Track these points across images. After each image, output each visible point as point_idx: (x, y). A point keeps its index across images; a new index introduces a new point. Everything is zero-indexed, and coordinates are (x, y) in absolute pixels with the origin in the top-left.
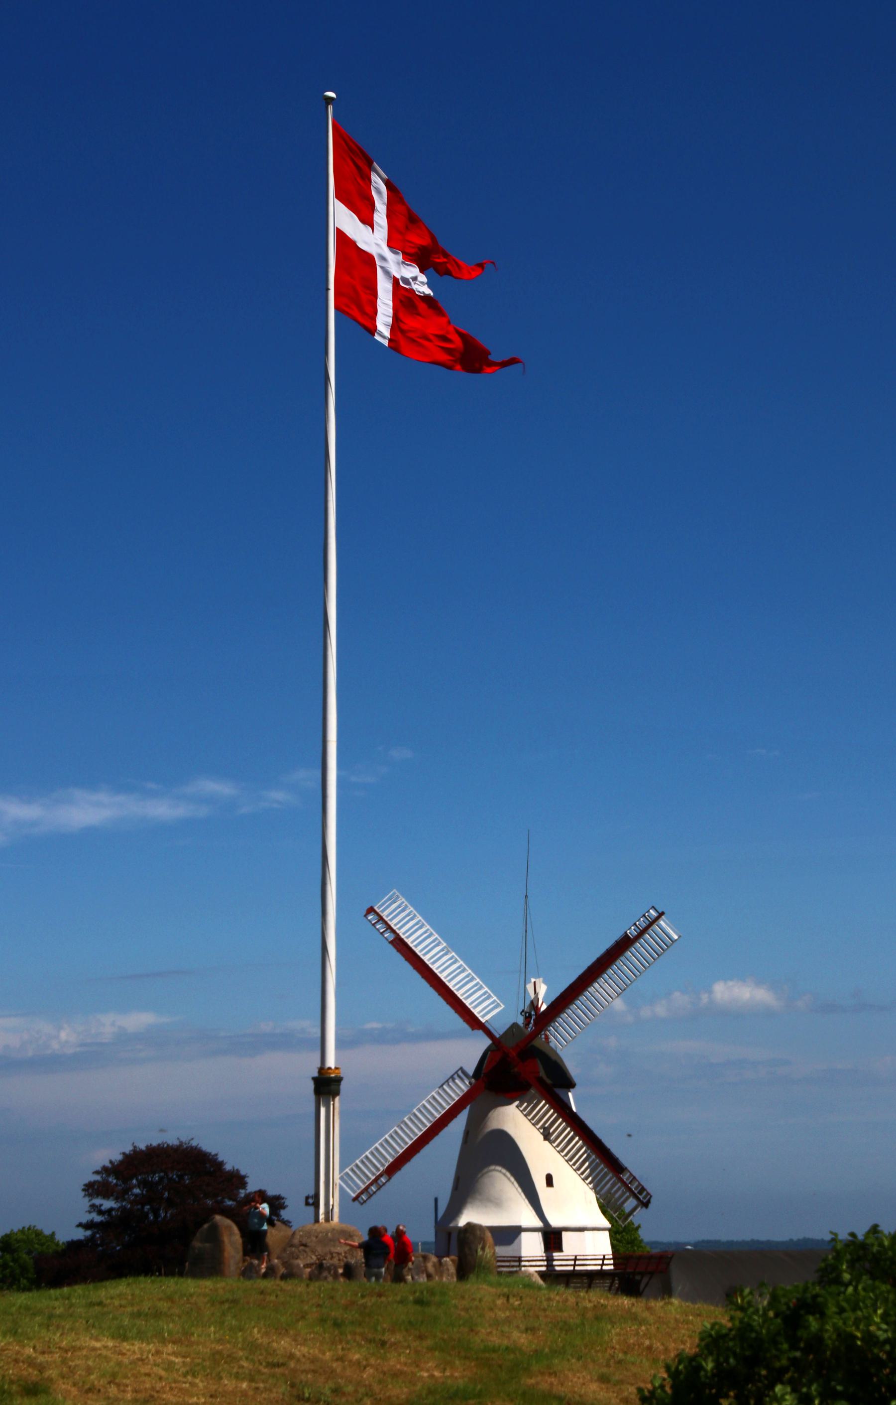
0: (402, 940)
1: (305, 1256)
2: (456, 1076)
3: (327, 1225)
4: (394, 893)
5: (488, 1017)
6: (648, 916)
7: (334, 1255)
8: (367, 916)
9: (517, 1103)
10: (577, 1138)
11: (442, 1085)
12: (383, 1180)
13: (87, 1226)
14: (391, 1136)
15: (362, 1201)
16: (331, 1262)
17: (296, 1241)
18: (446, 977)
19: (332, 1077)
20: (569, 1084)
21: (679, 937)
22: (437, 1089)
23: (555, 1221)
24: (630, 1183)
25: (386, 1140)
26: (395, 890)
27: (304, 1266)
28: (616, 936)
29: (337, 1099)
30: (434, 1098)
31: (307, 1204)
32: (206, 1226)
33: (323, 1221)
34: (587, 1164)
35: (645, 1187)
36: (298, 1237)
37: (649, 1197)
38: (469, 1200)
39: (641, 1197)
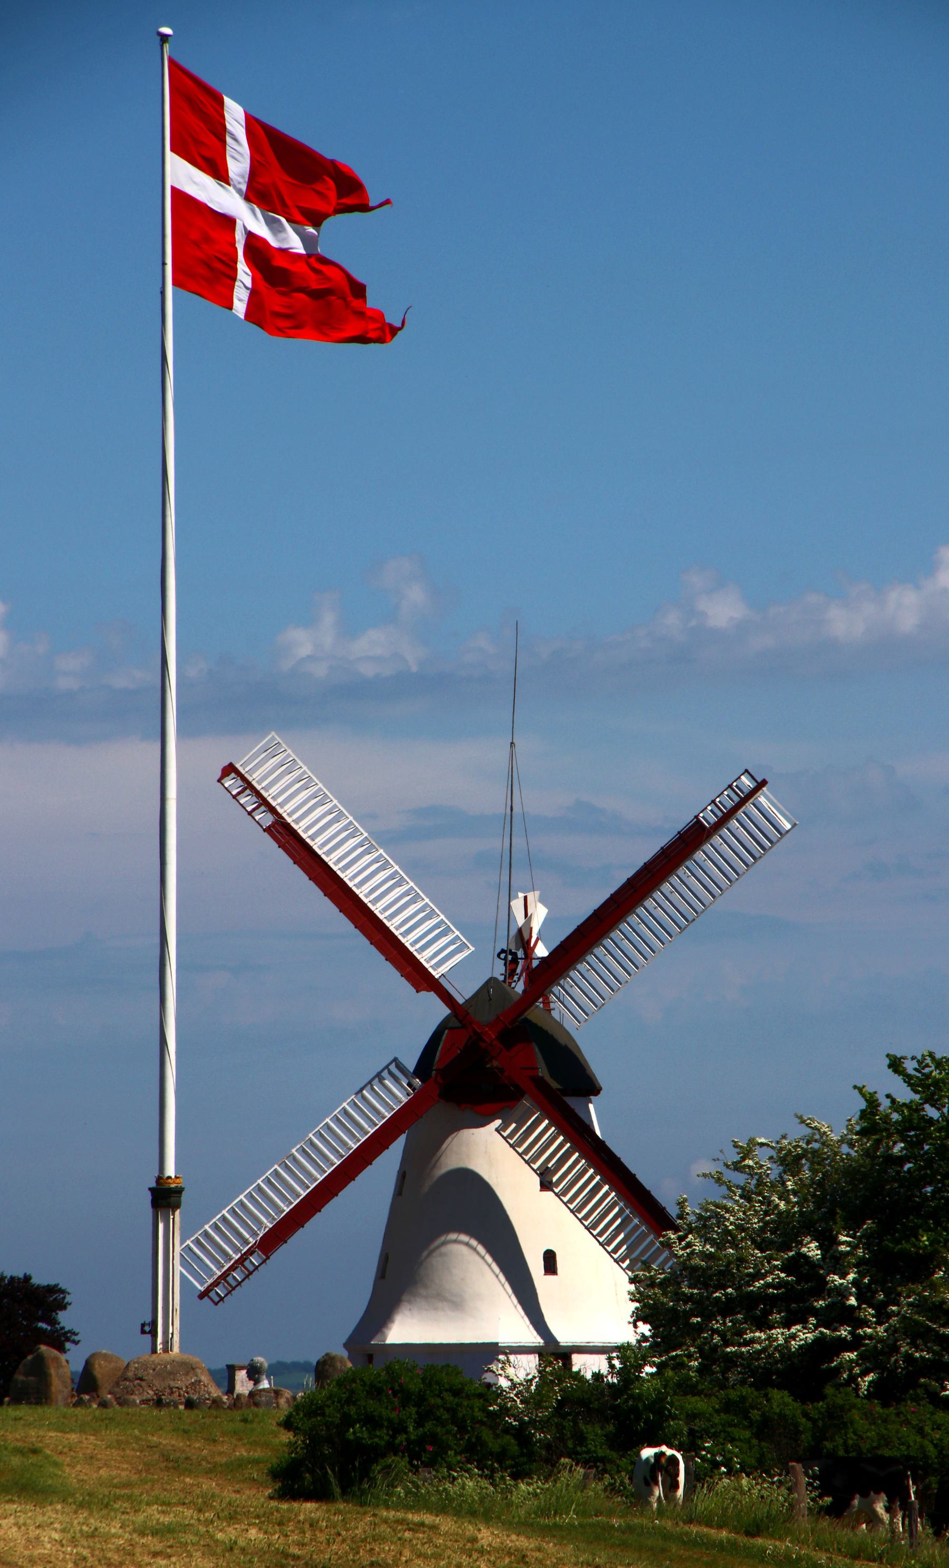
1: (141, 1391)
2: (385, 1074)
3: (165, 1356)
5: (444, 969)
6: (720, 802)
7: (174, 1390)
8: (222, 781)
9: (498, 1122)
10: (606, 1188)
11: (361, 1090)
12: (254, 1260)
14: (268, 1182)
15: (216, 1299)
16: (172, 1398)
17: (130, 1374)
19: (172, 1188)
20: (590, 1088)
21: (794, 825)
22: (353, 1097)
23: (564, 1336)
25: (259, 1189)
26: (273, 733)
27: (140, 1402)
29: (177, 1213)
31: (143, 1332)
32: (29, 1358)
33: (161, 1351)
34: (622, 1236)
36: (133, 1369)
38: (404, 1297)
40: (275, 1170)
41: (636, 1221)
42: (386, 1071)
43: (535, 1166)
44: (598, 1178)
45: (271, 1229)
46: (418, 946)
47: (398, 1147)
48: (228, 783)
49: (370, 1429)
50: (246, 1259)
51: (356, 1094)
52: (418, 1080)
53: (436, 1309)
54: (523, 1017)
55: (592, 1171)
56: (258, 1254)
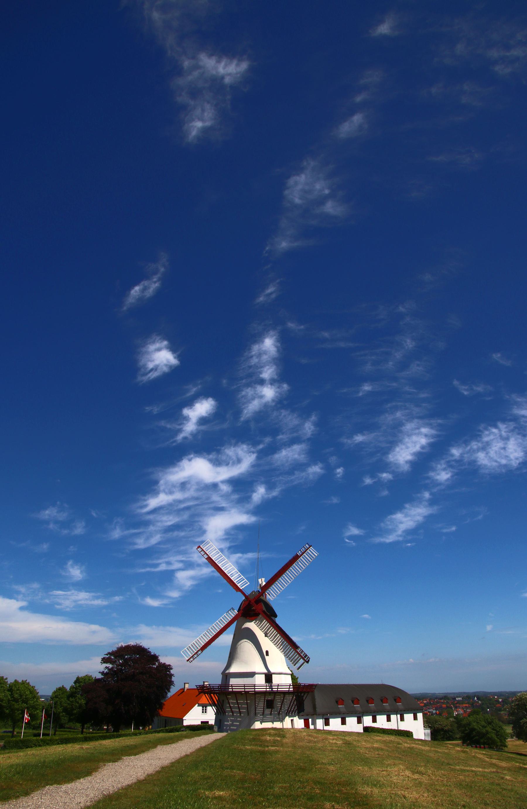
0: (210, 558)
5: (243, 587)
12: (200, 652)
13: (102, 673)
15: (190, 661)
18: (223, 569)
23: (272, 671)
34: (282, 646)
35: (307, 654)
39: (305, 659)
44: (277, 633)
48: (199, 549)
49: (413, 742)
55: (275, 631)
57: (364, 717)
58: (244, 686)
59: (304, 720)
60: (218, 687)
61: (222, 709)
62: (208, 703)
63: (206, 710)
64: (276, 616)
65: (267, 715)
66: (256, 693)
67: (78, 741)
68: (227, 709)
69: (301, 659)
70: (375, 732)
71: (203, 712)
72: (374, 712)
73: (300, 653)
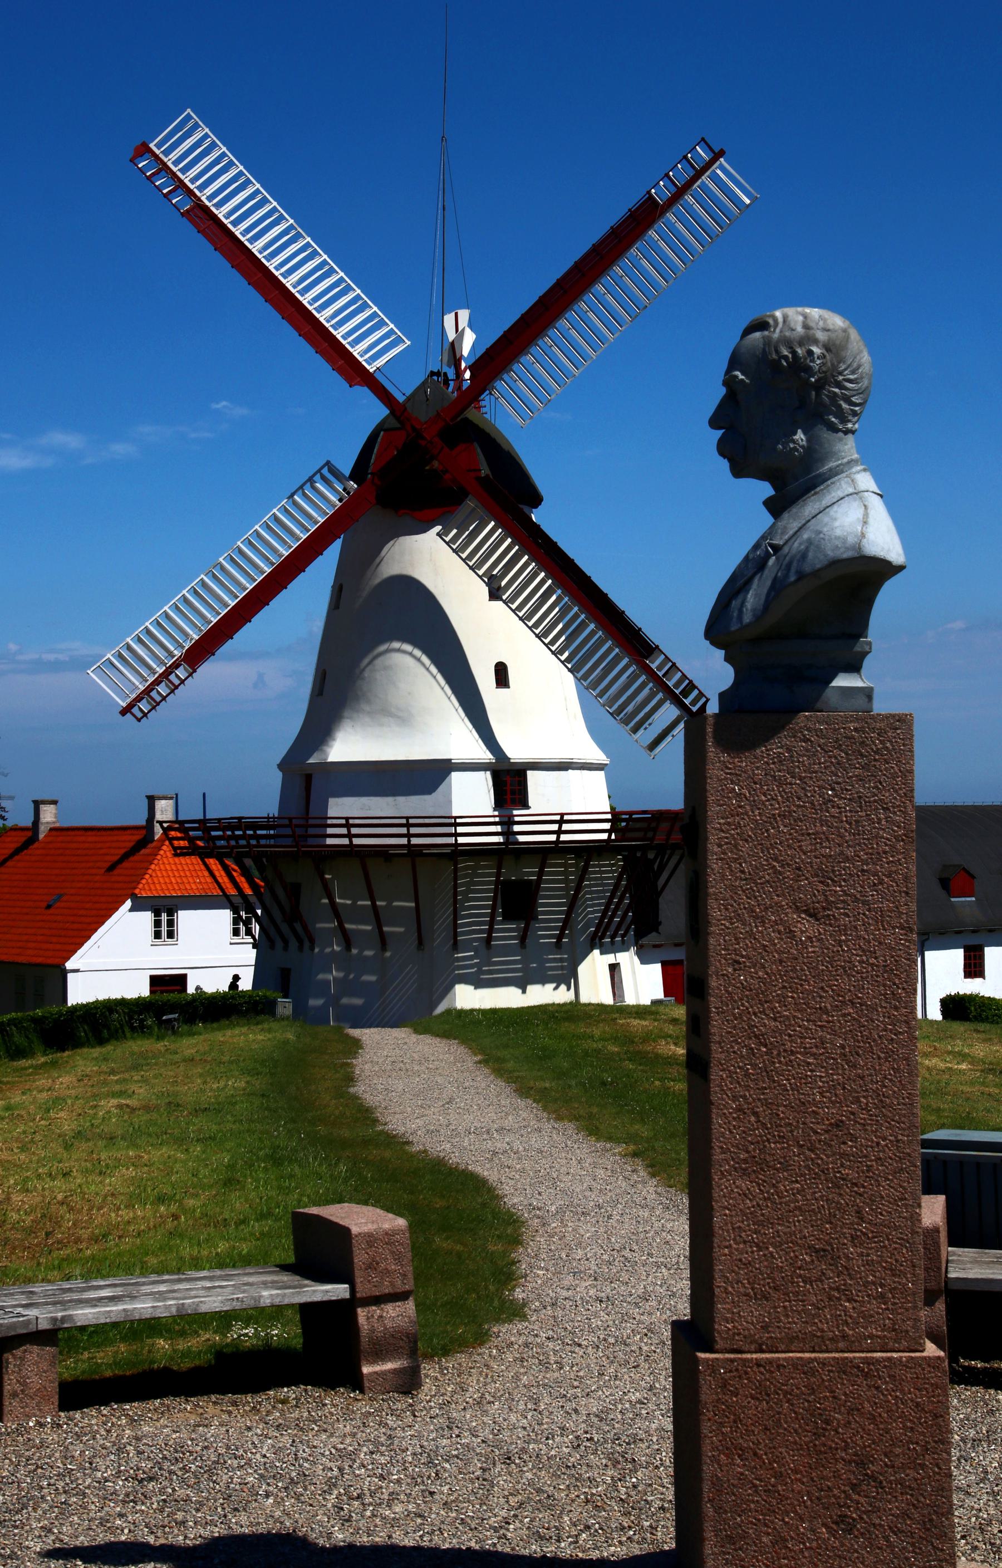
0: (206, 210)
2: (317, 477)
4: (189, 117)
5: (380, 362)
8: (135, 161)
9: (438, 528)
11: (292, 496)
12: (181, 673)
15: (139, 715)
23: (516, 752)
24: (664, 675)
26: (189, 110)
28: (632, 199)
30: (276, 519)
34: (560, 626)
35: (696, 683)
37: (704, 700)
38: (346, 713)
39: (687, 702)
40: (202, 579)
41: (592, 626)
42: (318, 476)
43: (481, 572)
44: (550, 582)
45: (197, 641)
46: (316, 305)
47: (332, 554)
50: (171, 673)
51: (289, 498)
52: (352, 483)
53: (381, 725)
54: (462, 416)
56: (185, 669)
57: (927, 953)
58: (348, 826)
59: (665, 965)
60: (259, 832)
61: (298, 926)
62: (217, 892)
63: (171, 923)
64: (535, 499)
65: (506, 951)
66: (457, 853)
67: (202, 1004)
68: (319, 925)
69: (667, 705)
70: (979, 1019)
71: (157, 935)
72: (974, 932)
73: (660, 674)
